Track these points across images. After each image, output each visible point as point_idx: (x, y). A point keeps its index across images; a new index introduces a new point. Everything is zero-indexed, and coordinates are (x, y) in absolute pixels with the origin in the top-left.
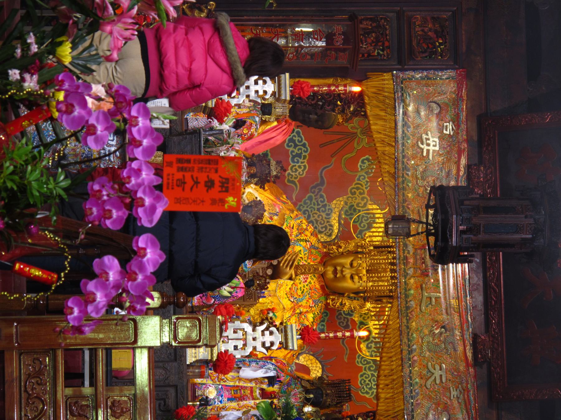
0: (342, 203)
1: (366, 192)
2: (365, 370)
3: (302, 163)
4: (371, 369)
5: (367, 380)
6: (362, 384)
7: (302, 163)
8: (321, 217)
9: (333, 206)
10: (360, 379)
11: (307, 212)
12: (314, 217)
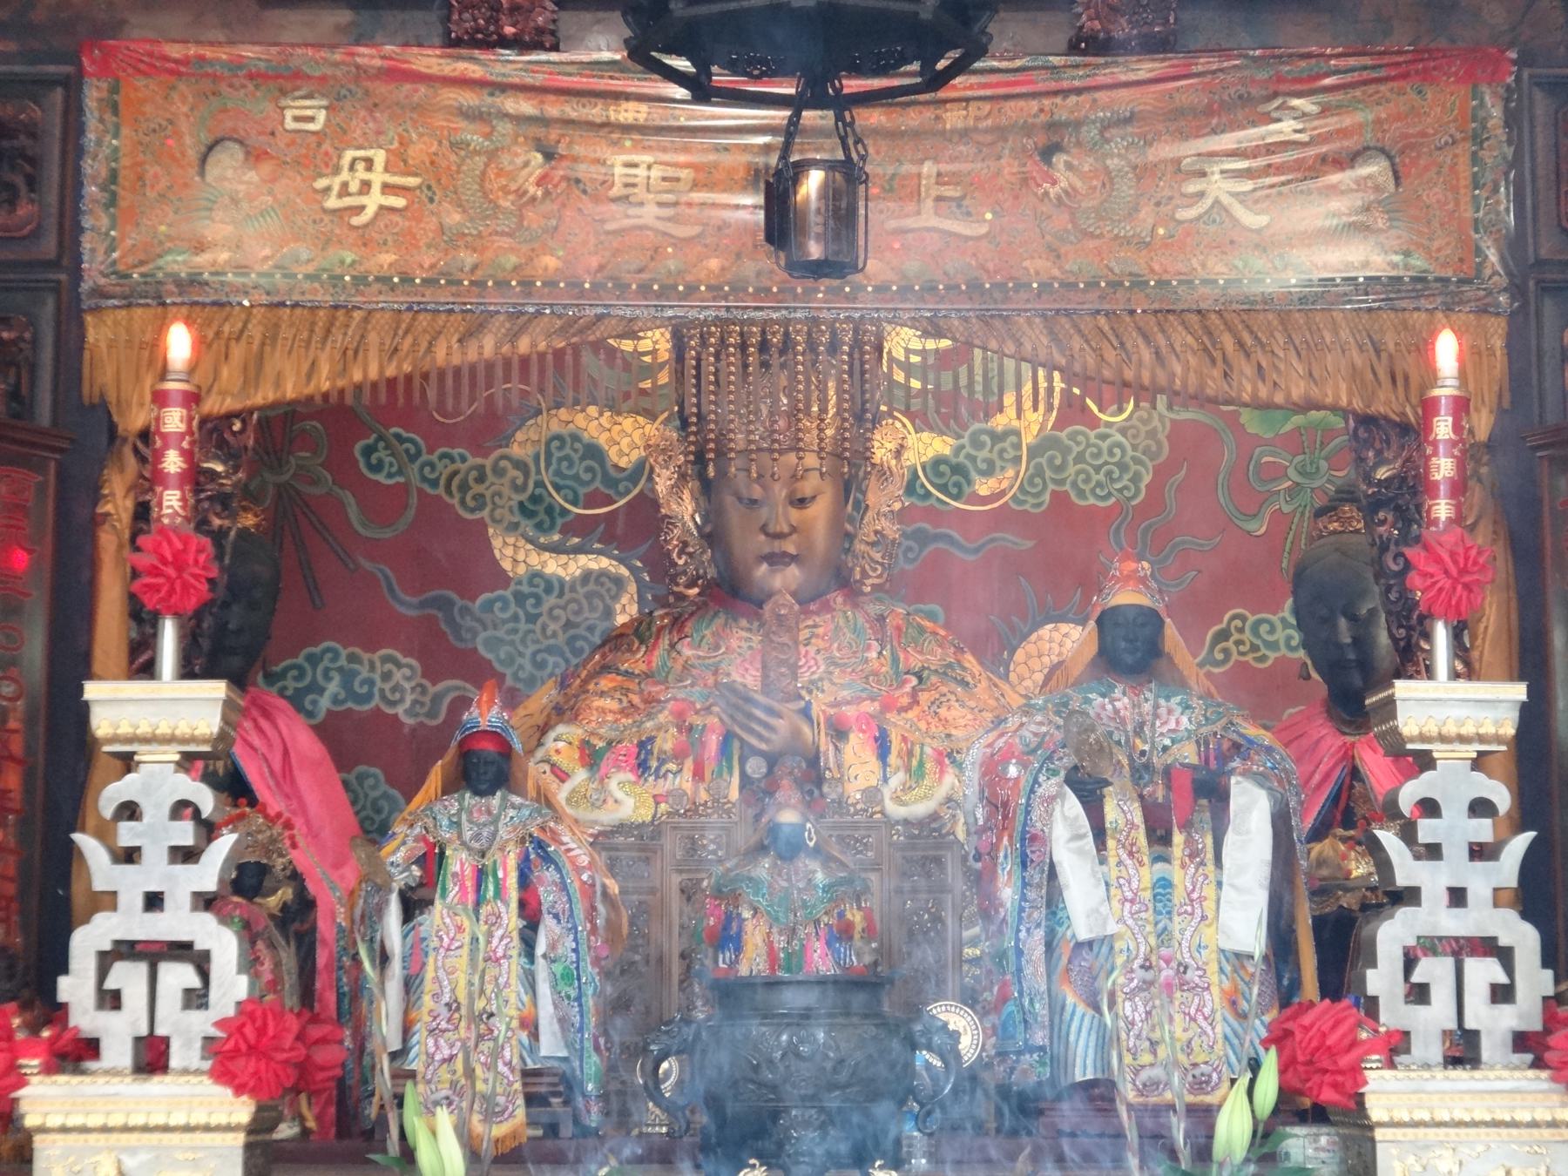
0: (511, 540)
1: (479, 461)
2: (1061, 482)
3: (372, 667)
4: (1058, 462)
5: (1095, 477)
6: (1110, 494)
7: (372, 667)
8: (557, 612)
9: (521, 569)
10: (1092, 501)
11: (539, 658)
12: (554, 635)
